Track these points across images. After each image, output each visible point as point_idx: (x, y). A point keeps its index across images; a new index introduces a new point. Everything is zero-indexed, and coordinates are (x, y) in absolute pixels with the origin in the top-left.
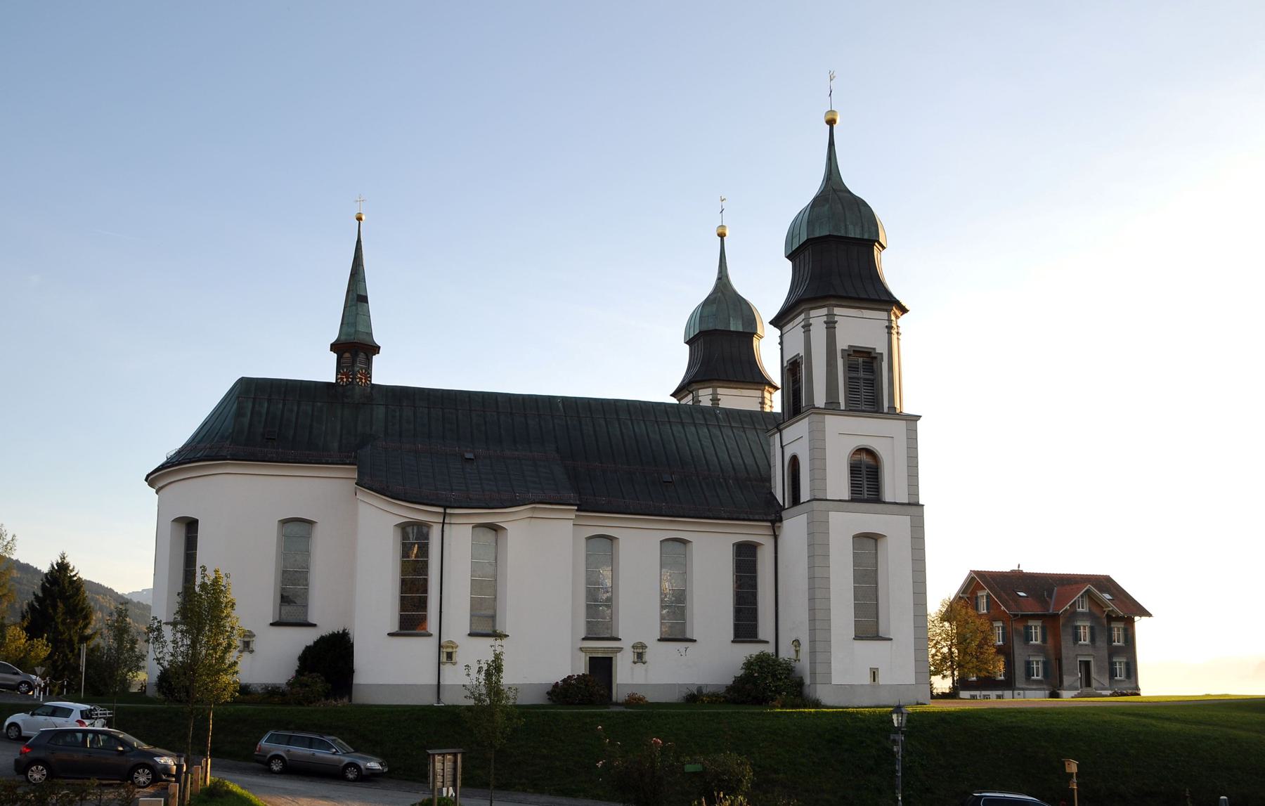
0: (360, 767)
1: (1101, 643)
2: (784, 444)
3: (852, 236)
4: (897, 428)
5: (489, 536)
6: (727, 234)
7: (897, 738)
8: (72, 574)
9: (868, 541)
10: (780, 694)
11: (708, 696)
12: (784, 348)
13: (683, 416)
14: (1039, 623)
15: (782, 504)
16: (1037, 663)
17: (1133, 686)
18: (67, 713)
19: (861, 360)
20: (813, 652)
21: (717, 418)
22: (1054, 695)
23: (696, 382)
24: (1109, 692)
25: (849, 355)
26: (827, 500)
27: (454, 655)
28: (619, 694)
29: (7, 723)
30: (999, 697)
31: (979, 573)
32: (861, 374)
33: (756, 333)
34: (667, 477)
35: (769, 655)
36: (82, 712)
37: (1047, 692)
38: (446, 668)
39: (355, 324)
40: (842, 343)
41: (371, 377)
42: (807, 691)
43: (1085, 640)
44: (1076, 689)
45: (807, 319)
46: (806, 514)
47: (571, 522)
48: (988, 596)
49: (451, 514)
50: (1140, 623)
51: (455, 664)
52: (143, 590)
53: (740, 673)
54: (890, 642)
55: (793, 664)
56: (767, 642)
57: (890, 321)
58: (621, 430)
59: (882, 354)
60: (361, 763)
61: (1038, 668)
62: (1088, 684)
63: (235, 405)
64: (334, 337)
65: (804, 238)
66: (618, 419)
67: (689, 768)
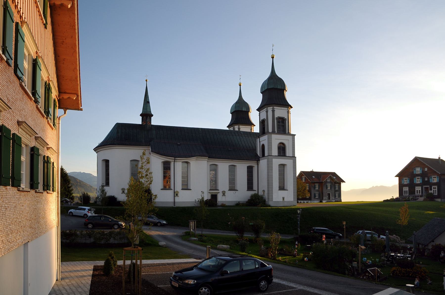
0: (161, 223)
1: (333, 189)
2: (260, 141)
3: (279, 88)
4: (290, 137)
5: (186, 165)
6: (242, 85)
7: (299, 216)
8: (64, 171)
9: (282, 167)
10: (260, 203)
11: (241, 204)
12: (260, 116)
13: (232, 133)
14: (318, 184)
15: (259, 156)
16: (317, 194)
17: (340, 199)
18: (85, 209)
19: (281, 120)
20: (268, 193)
21: (241, 134)
22: (321, 202)
23: (234, 124)
24: (334, 201)
25: (278, 119)
26: (272, 156)
27: (178, 194)
28: (219, 203)
29: (69, 212)
30: (307, 202)
31: (303, 172)
32: (281, 124)
33: (249, 111)
34: (229, 149)
35: (257, 194)
36: (88, 209)
37: (319, 201)
38: (176, 198)
39: (147, 109)
40: (276, 116)
41: (151, 123)
42: (267, 203)
43: (329, 188)
44: (326, 200)
45: (267, 109)
46: (267, 159)
47: (207, 161)
48: (305, 178)
49: (176, 159)
50: (342, 184)
51: (178, 196)
52: (71, 172)
53: (249, 198)
54: (287, 191)
55: (263, 196)
56: (256, 191)
57: (288, 110)
58: (217, 137)
59: (286, 119)
60: (161, 222)
61: (317, 195)
62: (329, 199)
63: (116, 130)
64: (141, 112)
65: (266, 88)
66: (216, 134)
67: (251, 224)
